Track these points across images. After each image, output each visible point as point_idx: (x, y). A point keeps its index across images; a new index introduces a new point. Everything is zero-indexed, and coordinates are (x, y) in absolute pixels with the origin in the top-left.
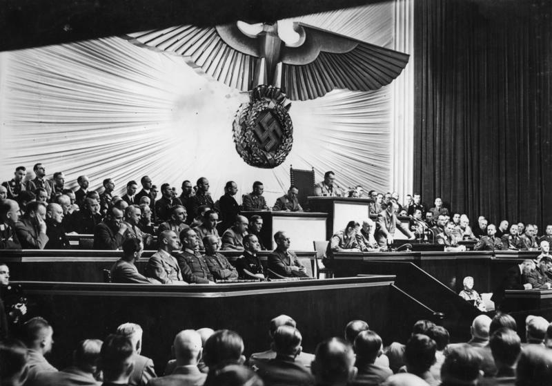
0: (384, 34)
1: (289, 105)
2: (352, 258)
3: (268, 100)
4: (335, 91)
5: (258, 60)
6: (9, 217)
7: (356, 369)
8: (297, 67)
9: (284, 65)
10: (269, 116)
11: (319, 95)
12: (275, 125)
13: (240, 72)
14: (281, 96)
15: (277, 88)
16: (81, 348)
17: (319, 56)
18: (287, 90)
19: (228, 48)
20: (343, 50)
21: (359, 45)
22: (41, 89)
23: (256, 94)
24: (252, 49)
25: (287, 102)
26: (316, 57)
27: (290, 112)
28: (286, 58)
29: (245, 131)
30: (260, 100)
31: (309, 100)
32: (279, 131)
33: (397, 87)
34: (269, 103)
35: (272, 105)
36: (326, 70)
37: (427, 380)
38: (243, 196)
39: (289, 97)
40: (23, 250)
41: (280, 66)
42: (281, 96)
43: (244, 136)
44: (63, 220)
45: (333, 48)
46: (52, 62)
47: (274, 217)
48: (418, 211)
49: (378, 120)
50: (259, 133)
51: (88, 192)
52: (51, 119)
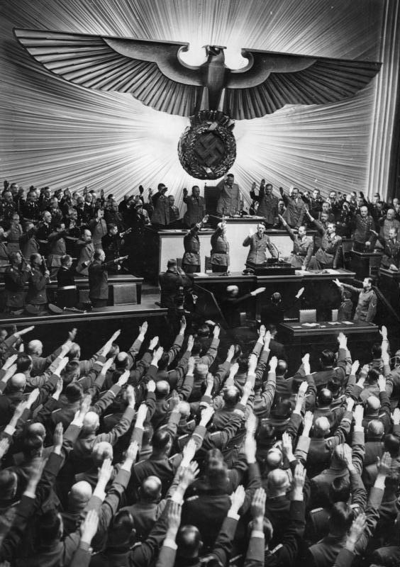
0: (363, 42)
3: (209, 123)
4: (286, 106)
7: (237, 517)
8: (250, 89)
9: (228, 91)
11: (268, 113)
12: (216, 143)
16: (76, 327)
17: (269, 77)
18: (231, 113)
21: (317, 62)
22: (15, 126)
24: (194, 80)
25: (232, 122)
26: (265, 79)
27: (234, 131)
28: (232, 83)
31: (246, 120)
32: (221, 149)
33: (381, 77)
35: (214, 126)
36: (277, 89)
44: (52, 221)
45: (285, 68)
46: (25, 104)
48: (137, 498)
51: (5, 231)
52: (24, 148)
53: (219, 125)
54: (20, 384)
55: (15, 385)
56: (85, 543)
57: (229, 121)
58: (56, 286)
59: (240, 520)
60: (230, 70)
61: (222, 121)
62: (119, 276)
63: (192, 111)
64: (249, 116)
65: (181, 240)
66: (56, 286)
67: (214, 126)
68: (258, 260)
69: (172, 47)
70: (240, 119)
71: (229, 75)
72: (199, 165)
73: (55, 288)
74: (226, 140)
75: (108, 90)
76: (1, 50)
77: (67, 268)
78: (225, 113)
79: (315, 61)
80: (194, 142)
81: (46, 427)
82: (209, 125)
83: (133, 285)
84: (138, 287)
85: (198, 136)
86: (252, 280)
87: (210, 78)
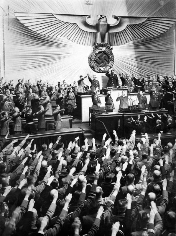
1: (112, 49)
2: (114, 116)
5: (97, 34)
13: (89, 39)
14: (107, 46)
19: (87, 33)
20: (136, 23)
25: (111, 47)
27: (113, 51)
29: (91, 61)
30: (97, 49)
37: (84, 20)
38: (90, 108)
39: (112, 46)
40: (29, 123)
41: (107, 34)
42: (107, 46)
47: (82, 98)
53: (106, 49)
54: (45, 166)
55: (43, 166)
56: (77, 235)
57: (110, 47)
58: (25, 123)
59: (68, 211)
60: (109, 25)
61: (107, 47)
62: (64, 116)
63: (94, 44)
64: (119, 44)
65: (91, 99)
66: (25, 123)
67: (104, 49)
68: (125, 107)
69: (83, 16)
70: (115, 46)
71: (109, 27)
72: (98, 67)
73: (24, 124)
74: (109, 55)
75: (64, 37)
76: (134, 0)
77: (30, 114)
78: (108, 43)
79: (147, 18)
80: (95, 57)
81: (102, 188)
82: (101, 49)
83: (68, 120)
84: (70, 121)
85: (96, 54)
86: (121, 115)
87: (101, 29)
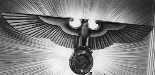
0: (146, 18)
3: (82, 51)
4: (114, 44)
6: (78, 55)
8: (99, 37)
9: (90, 38)
10: (82, 57)
11: (106, 47)
12: (85, 59)
15: (86, 47)
17: (107, 32)
18: (91, 47)
21: (127, 26)
23: (77, 49)
24: (76, 33)
26: (105, 33)
27: (92, 54)
28: (91, 35)
31: (97, 50)
32: (87, 62)
34: (82, 52)
35: (84, 52)
36: (110, 37)
43: (71, 64)
45: (114, 28)
46: (6, 43)
49: (146, 46)
50: (78, 63)
52: (5, 61)
